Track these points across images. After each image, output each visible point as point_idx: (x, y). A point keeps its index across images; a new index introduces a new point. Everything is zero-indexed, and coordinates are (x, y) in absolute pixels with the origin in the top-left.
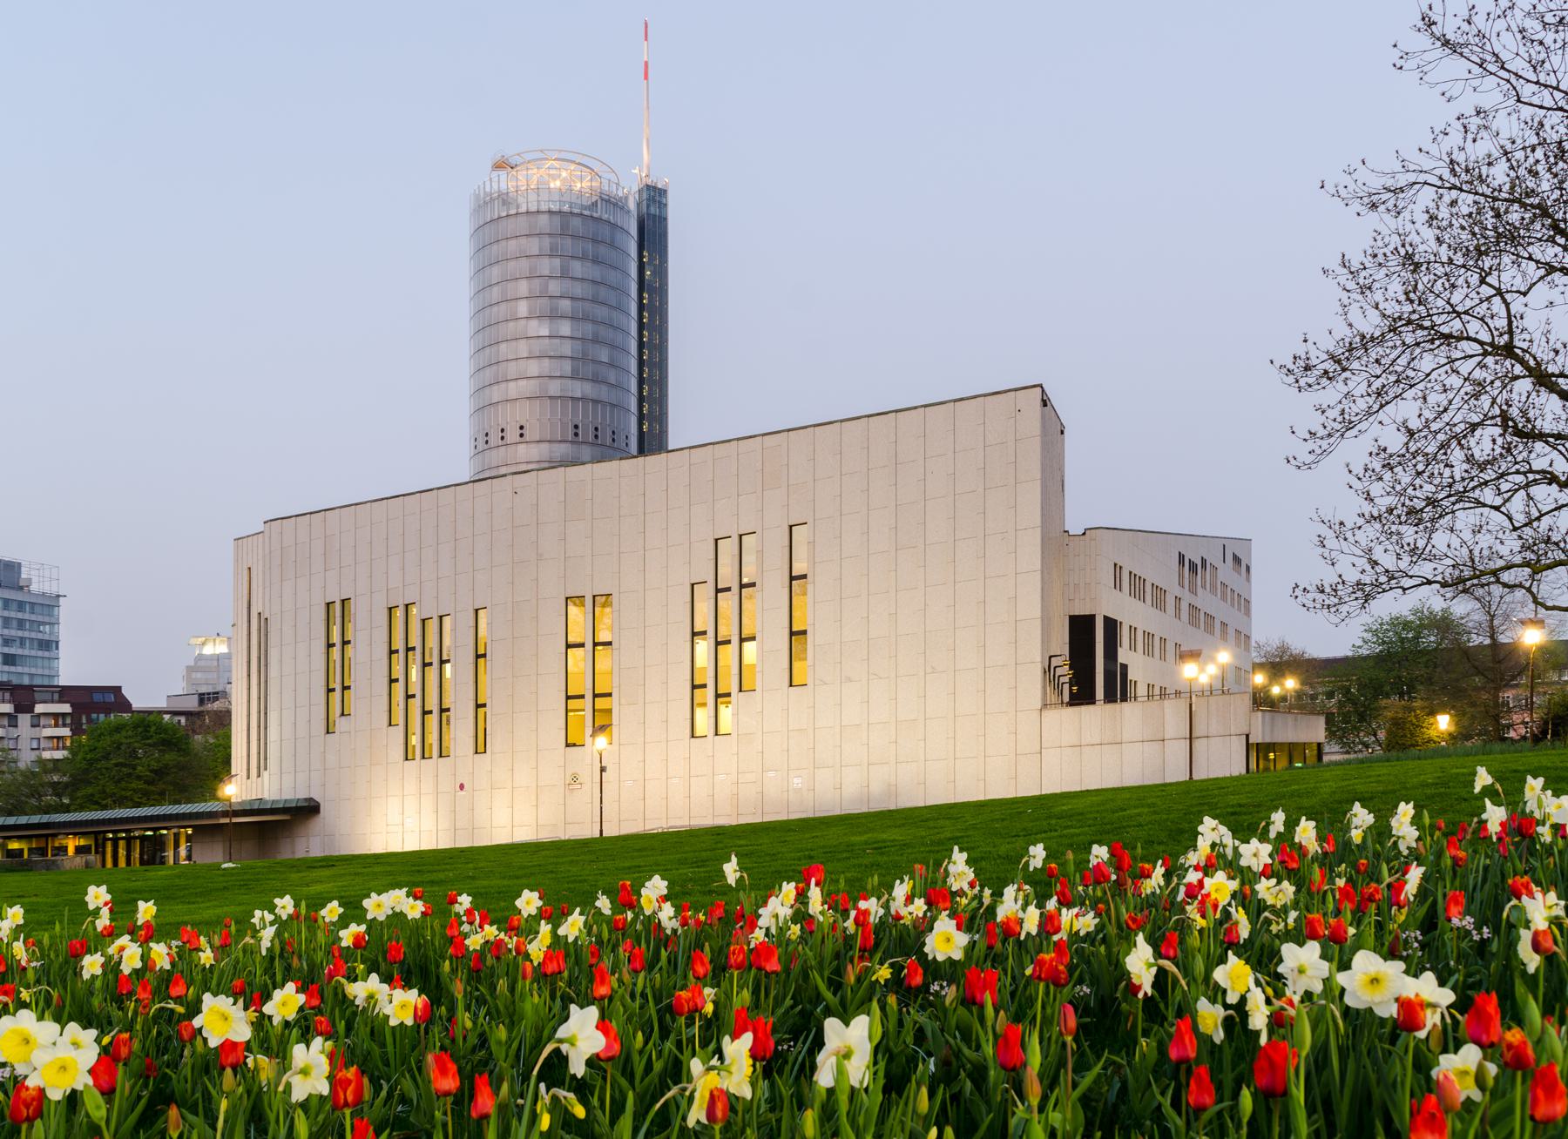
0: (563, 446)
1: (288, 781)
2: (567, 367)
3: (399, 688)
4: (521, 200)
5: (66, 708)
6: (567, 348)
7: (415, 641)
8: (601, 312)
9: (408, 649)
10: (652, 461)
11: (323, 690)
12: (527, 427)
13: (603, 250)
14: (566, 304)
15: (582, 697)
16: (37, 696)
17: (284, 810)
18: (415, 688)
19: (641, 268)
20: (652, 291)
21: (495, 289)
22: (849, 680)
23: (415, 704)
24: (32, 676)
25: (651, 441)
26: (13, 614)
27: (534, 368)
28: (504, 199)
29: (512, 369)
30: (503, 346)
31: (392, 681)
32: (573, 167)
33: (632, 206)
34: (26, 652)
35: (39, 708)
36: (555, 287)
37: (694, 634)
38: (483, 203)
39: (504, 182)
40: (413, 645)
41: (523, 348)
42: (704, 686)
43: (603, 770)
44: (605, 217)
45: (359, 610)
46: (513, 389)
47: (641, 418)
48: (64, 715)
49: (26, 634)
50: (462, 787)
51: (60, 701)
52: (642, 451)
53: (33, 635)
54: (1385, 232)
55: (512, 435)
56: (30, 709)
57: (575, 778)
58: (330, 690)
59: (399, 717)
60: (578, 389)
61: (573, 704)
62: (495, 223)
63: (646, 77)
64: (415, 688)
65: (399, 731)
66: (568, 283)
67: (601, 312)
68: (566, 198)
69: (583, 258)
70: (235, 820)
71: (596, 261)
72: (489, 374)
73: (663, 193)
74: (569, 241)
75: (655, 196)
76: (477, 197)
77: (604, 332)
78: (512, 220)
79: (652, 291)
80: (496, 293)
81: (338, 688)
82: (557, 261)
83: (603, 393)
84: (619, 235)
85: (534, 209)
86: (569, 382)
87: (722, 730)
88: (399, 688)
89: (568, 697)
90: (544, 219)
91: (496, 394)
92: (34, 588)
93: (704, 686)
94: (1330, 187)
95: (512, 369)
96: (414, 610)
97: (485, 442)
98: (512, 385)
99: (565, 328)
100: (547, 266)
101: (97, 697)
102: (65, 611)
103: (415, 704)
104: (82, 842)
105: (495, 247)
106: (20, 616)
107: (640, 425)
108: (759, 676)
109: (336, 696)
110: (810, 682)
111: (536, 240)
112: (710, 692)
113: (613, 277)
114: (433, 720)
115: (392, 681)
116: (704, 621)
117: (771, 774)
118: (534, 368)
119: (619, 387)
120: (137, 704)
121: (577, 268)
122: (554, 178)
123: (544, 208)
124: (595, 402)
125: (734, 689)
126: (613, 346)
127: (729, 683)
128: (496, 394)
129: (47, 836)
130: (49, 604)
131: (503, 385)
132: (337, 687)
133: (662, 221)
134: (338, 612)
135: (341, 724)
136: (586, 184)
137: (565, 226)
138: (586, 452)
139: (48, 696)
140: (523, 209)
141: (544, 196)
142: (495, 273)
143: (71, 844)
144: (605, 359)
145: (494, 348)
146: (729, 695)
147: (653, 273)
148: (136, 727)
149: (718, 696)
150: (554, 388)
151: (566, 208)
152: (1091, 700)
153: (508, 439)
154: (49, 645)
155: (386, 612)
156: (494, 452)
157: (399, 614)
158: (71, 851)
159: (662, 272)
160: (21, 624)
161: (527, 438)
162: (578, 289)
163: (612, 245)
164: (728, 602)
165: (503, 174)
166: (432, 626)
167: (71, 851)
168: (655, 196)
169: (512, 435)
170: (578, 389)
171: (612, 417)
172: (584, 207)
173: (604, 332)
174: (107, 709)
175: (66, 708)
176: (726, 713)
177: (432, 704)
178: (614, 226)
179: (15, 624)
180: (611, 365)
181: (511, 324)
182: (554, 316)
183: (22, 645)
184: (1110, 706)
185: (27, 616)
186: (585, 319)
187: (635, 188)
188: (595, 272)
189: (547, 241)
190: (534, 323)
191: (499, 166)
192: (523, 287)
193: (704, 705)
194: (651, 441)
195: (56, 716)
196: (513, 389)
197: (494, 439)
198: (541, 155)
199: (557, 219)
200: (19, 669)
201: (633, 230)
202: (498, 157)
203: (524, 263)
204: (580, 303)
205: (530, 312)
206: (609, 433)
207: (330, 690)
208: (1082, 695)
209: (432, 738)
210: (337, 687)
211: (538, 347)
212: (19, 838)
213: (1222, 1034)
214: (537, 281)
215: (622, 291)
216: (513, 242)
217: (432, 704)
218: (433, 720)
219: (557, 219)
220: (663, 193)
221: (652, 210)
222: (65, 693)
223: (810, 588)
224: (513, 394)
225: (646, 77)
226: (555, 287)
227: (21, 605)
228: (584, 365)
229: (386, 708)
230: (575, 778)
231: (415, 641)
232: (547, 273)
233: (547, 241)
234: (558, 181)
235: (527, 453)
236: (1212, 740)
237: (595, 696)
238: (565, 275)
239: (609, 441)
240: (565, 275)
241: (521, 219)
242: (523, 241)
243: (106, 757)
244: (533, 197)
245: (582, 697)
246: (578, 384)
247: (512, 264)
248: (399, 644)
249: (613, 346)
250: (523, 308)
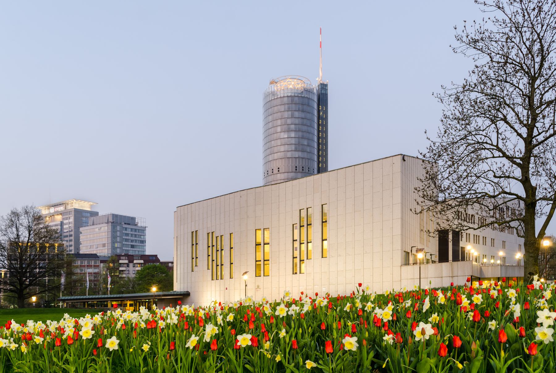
0: (292, 173)
1: (182, 287)
2: (293, 147)
3: (210, 258)
4: (278, 93)
5: (142, 261)
6: (293, 141)
7: (214, 244)
8: (305, 128)
9: (213, 246)
10: (324, 175)
11: (207, 255)
12: (280, 168)
13: (305, 107)
14: (293, 127)
15: (260, 261)
16: (135, 258)
17: (180, 295)
18: (214, 258)
19: (319, 111)
20: (323, 119)
21: (270, 123)
22: (340, 256)
23: (215, 262)
24: (138, 251)
25: (322, 168)
26: (133, 233)
27: (282, 148)
28: (273, 94)
29: (276, 149)
30: (273, 142)
31: (209, 256)
32: (295, 80)
33: (315, 91)
34: (137, 244)
35: (135, 262)
36: (289, 121)
37: (294, 241)
38: (267, 95)
39: (274, 88)
40: (216, 246)
41: (279, 142)
42: (296, 257)
43: (246, 286)
44: (306, 96)
45: (200, 234)
46: (276, 156)
47: (319, 162)
48: (142, 263)
49: (137, 239)
50: (227, 289)
51: (141, 259)
52: (319, 172)
53: (139, 239)
54: (446, 110)
55: (276, 171)
56: (132, 262)
57: (258, 287)
58: (193, 258)
59: (210, 267)
60: (297, 154)
61: (258, 263)
62: (271, 102)
63: (321, 47)
64: (214, 258)
65: (210, 271)
66: (293, 119)
67: (305, 128)
68: (293, 91)
69: (299, 110)
70: (163, 297)
71: (303, 111)
72: (268, 151)
73: (326, 85)
74: (294, 105)
75: (324, 87)
76: (265, 94)
77: (306, 135)
78: (276, 100)
79: (323, 119)
80: (270, 125)
81: (195, 258)
82: (290, 113)
83: (305, 155)
84: (311, 102)
85: (282, 96)
86: (294, 152)
87: (302, 271)
88: (210, 258)
89: (256, 261)
90: (286, 99)
91: (271, 158)
92: (139, 225)
93: (296, 257)
94: (435, 95)
95: (276, 149)
96: (214, 234)
97: (268, 173)
98: (276, 154)
99: (293, 134)
100: (286, 114)
101: (151, 258)
102: (147, 232)
103: (215, 262)
104: (132, 302)
105: (270, 110)
106: (135, 233)
107: (318, 164)
108: (312, 254)
109: (194, 260)
110: (328, 256)
111: (283, 106)
112: (298, 259)
113: (309, 116)
114: (219, 267)
115: (209, 256)
116: (296, 237)
117: (316, 286)
118: (282, 148)
119: (311, 153)
121: (297, 114)
122: (290, 84)
123: (286, 95)
124: (302, 158)
125: (305, 258)
126: (308, 139)
127: (304, 257)
128: (271, 158)
129: (122, 301)
130: (143, 230)
131: (273, 155)
132: (194, 258)
133: (326, 95)
134: (195, 234)
135: (195, 269)
136: (300, 86)
137: (292, 101)
138: (299, 175)
139: (137, 258)
140: (279, 97)
141: (286, 91)
142: (270, 118)
143: (129, 303)
144: (306, 143)
145: (270, 143)
146: (303, 260)
147: (323, 113)
148: (153, 268)
149: (301, 261)
150: (289, 155)
151: (293, 95)
152: (447, 260)
153: (269, 174)
154: (143, 242)
155: (207, 235)
156: (270, 177)
157: (210, 235)
158: (128, 305)
159: (326, 112)
160: (135, 236)
161: (280, 172)
162: (297, 121)
163: (308, 105)
164: (304, 230)
165: (272, 85)
166: (219, 239)
167: (128, 305)
168: (324, 87)
169: (276, 171)
170: (297, 154)
171: (305, 163)
172: (300, 94)
173: (306, 135)
174: (153, 261)
175: (142, 261)
176: (303, 266)
177: (219, 263)
178: (309, 99)
179: (134, 236)
180: (308, 145)
181: (275, 135)
182: (289, 131)
183: (136, 242)
184: (455, 263)
185: (137, 233)
187: (317, 85)
188: (303, 115)
189: (286, 106)
190: (282, 134)
191: (271, 83)
192: (279, 122)
194: (322, 168)
195: (139, 264)
196: (276, 156)
197: (270, 173)
198: (285, 78)
199: (290, 98)
200: (135, 249)
201: (316, 99)
202: (271, 80)
203: (279, 114)
204: (297, 126)
205: (281, 130)
206: (307, 168)
207: (193, 258)
208: (443, 257)
209: (219, 273)
210: (194, 258)
211: (283, 141)
212: (115, 301)
214: (283, 120)
215: (312, 120)
216: (276, 108)
217: (219, 263)
218: (219, 267)
219: (290, 98)
220: (326, 85)
221: (323, 92)
222: (143, 257)
223: (328, 225)
224: (276, 158)
225: (321, 47)
226: (289, 121)
227: (136, 230)
228: (299, 147)
229: (321, 251)
230: (258, 287)
231: (214, 244)
232: (287, 116)
233: (286, 106)
234: (292, 85)
235: (280, 176)
236: (459, 277)
237: (264, 260)
238: (292, 117)
239: (307, 171)
240: (292, 117)
241: (279, 100)
242: (279, 107)
243: (145, 277)
244: (282, 92)
245: (260, 261)
246: (297, 153)
247: (275, 115)
248: (210, 245)
249: (308, 139)
250: (279, 129)
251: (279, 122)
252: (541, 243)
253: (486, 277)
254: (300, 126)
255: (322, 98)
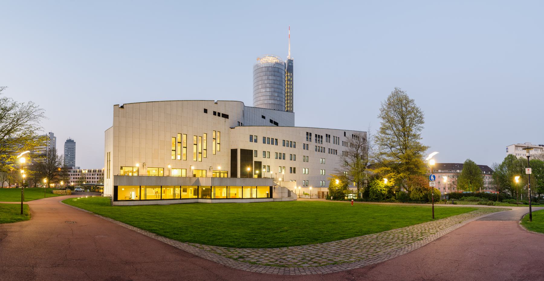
2: (268, 97)
6: (268, 94)
13: (276, 73)
14: (268, 85)
36: (266, 82)
60: (271, 102)
62: (258, 70)
69: (272, 75)
71: (274, 76)
73: (292, 61)
75: (290, 61)
90: (264, 68)
99: (268, 90)
100: (264, 78)
118: (262, 98)
120: (463, 163)
121: (270, 77)
124: (274, 104)
133: (292, 66)
134: (234, 152)
162: (271, 82)
168: (290, 61)
182: (266, 87)
186: (272, 87)
188: (274, 78)
192: (260, 82)
193: (149, 172)
213: (39, 186)
220: (292, 61)
234: (271, 60)
238: (268, 79)
240: (268, 79)
250: (260, 87)
251: (260, 82)
252: (515, 185)
253: (529, 211)
254: (273, 85)
255: (290, 67)
